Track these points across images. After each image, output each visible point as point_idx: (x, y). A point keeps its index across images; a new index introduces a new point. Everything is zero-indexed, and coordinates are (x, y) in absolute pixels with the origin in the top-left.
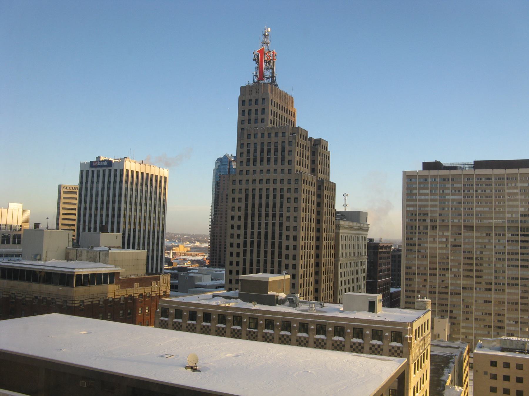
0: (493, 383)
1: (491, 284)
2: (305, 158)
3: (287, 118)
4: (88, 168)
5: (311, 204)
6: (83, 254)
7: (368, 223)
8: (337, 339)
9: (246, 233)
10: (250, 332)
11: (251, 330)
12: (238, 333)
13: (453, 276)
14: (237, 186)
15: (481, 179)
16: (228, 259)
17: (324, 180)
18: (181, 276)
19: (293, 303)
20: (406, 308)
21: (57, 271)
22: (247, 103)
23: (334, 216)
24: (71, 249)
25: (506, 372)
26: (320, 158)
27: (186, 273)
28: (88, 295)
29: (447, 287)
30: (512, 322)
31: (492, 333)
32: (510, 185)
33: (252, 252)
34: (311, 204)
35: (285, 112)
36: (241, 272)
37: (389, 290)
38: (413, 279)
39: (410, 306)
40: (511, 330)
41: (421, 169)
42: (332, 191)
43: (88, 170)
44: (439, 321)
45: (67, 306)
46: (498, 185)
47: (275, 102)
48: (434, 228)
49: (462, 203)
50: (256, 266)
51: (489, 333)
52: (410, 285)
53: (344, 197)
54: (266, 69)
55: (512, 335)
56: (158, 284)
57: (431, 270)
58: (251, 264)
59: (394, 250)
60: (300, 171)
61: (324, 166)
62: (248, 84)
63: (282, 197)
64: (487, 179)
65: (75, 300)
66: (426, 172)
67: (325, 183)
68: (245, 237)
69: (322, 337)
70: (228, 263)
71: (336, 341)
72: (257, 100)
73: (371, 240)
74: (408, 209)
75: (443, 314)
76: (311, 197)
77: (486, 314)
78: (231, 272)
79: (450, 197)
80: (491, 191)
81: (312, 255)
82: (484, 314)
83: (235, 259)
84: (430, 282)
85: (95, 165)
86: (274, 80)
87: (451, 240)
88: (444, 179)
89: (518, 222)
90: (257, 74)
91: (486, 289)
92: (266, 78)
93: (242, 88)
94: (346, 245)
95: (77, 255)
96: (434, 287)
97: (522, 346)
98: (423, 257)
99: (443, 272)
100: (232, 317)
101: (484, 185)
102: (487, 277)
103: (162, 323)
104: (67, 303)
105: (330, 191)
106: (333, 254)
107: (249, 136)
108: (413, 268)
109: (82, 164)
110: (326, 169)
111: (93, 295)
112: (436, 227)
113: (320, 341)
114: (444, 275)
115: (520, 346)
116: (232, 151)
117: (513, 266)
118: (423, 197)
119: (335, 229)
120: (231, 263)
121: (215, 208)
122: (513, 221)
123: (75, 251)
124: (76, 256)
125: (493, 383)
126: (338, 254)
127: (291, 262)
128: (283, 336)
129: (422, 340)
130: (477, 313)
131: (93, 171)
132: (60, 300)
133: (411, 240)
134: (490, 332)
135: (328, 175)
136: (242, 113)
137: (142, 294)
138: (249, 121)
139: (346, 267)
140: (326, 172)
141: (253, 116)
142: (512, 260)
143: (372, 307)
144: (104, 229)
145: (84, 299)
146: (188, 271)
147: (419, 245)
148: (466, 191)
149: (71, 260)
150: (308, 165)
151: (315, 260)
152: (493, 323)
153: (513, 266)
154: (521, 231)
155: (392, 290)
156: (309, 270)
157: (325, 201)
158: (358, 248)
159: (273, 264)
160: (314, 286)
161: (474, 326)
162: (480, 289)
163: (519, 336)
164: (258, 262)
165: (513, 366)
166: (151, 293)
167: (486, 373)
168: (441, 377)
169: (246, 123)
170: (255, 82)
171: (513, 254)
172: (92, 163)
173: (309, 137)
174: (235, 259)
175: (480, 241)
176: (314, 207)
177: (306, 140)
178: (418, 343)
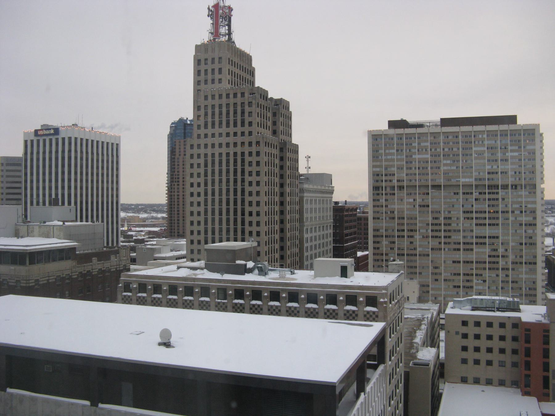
0: (465, 342)
1: (460, 243)
2: (266, 120)
3: (245, 78)
4: (32, 137)
5: (274, 167)
6: (35, 230)
7: (333, 185)
8: (311, 307)
9: (206, 201)
10: (219, 303)
11: (219, 301)
12: (207, 305)
13: (421, 237)
14: (195, 151)
15: (448, 137)
16: (188, 228)
17: (286, 142)
18: (139, 248)
19: (262, 272)
20: (374, 271)
21: (8, 249)
22: (203, 62)
23: (297, 179)
24: (22, 225)
25: (477, 330)
26: (281, 119)
27: (143, 245)
28: (43, 274)
29: (415, 249)
30: (480, 281)
31: (461, 293)
32: (477, 143)
33: (213, 220)
34: (274, 167)
35: (243, 71)
36: (203, 242)
37: (356, 254)
38: (381, 242)
39: (379, 269)
40: (479, 289)
41: (386, 127)
42: (295, 153)
43: (33, 140)
44: (408, 284)
45: (21, 286)
46: (466, 143)
47: (232, 60)
48: (401, 188)
49: (429, 162)
50: (218, 235)
51: (457, 293)
52: (378, 248)
53: (306, 159)
54: (222, 26)
55: (480, 294)
56: (118, 257)
57: (399, 232)
58: (213, 233)
59: (359, 213)
60: (284, 140)
61: (264, 119)
62: (203, 42)
63: (243, 161)
64: (454, 137)
65: (29, 280)
66: (392, 131)
67: (287, 145)
68: (206, 205)
69: (295, 305)
70: (188, 232)
71: (309, 309)
72: (213, 59)
73: (336, 203)
74: (374, 169)
75: (412, 276)
76: (274, 160)
77: (455, 274)
78: (192, 242)
79: (417, 157)
80: (458, 149)
81: (277, 221)
82: (452, 274)
83: (195, 228)
84: (398, 244)
85: (40, 133)
86: (231, 37)
87: (418, 200)
88: (409, 137)
89: (486, 180)
90: (213, 32)
91: (455, 250)
92: (222, 35)
93: (197, 47)
94: (311, 209)
95: (29, 231)
96: (402, 250)
97: (492, 304)
98: (390, 218)
99: (411, 234)
100: (200, 289)
101: (451, 143)
102: (455, 237)
103: (125, 299)
104: (20, 283)
105: (293, 153)
106: (297, 219)
107: (206, 98)
108: (381, 230)
109: (25, 134)
110: (288, 130)
111: (49, 272)
112: (403, 188)
113: (292, 309)
114: (412, 237)
115: (491, 305)
116: (189, 114)
117: (481, 225)
118: (389, 157)
119: (300, 192)
120: (192, 233)
121: (171, 176)
122: (480, 179)
123: (26, 227)
124: (28, 232)
125: (465, 342)
126: (303, 219)
127: (254, 229)
128: (254, 305)
129: (396, 303)
130: (446, 274)
131: (38, 141)
132: (13, 281)
133: (378, 202)
134: (459, 293)
135: (290, 137)
136: (198, 73)
137: (101, 269)
138: (206, 82)
139: (311, 232)
140: (288, 133)
141: (210, 77)
142: (480, 218)
143: (344, 272)
144: (54, 202)
145: (39, 278)
146: (146, 243)
147: (386, 206)
148: (433, 150)
149: (22, 237)
150: (269, 127)
151: (279, 225)
152: (461, 283)
153: (481, 225)
154: (488, 189)
155: (359, 254)
156: (274, 237)
157: (288, 163)
158: (323, 212)
159: (237, 231)
160: (279, 253)
161: (443, 287)
162: (449, 249)
163: (487, 295)
164: (221, 230)
165: (483, 324)
166: (110, 268)
167: (457, 333)
168: (414, 339)
169: (202, 83)
170: (210, 40)
171: (481, 212)
172: (36, 131)
173: (269, 97)
174: (195, 228)
175: (448, 200)
176: (277, 170)
177: (266, 100)
178: (393, 306)
